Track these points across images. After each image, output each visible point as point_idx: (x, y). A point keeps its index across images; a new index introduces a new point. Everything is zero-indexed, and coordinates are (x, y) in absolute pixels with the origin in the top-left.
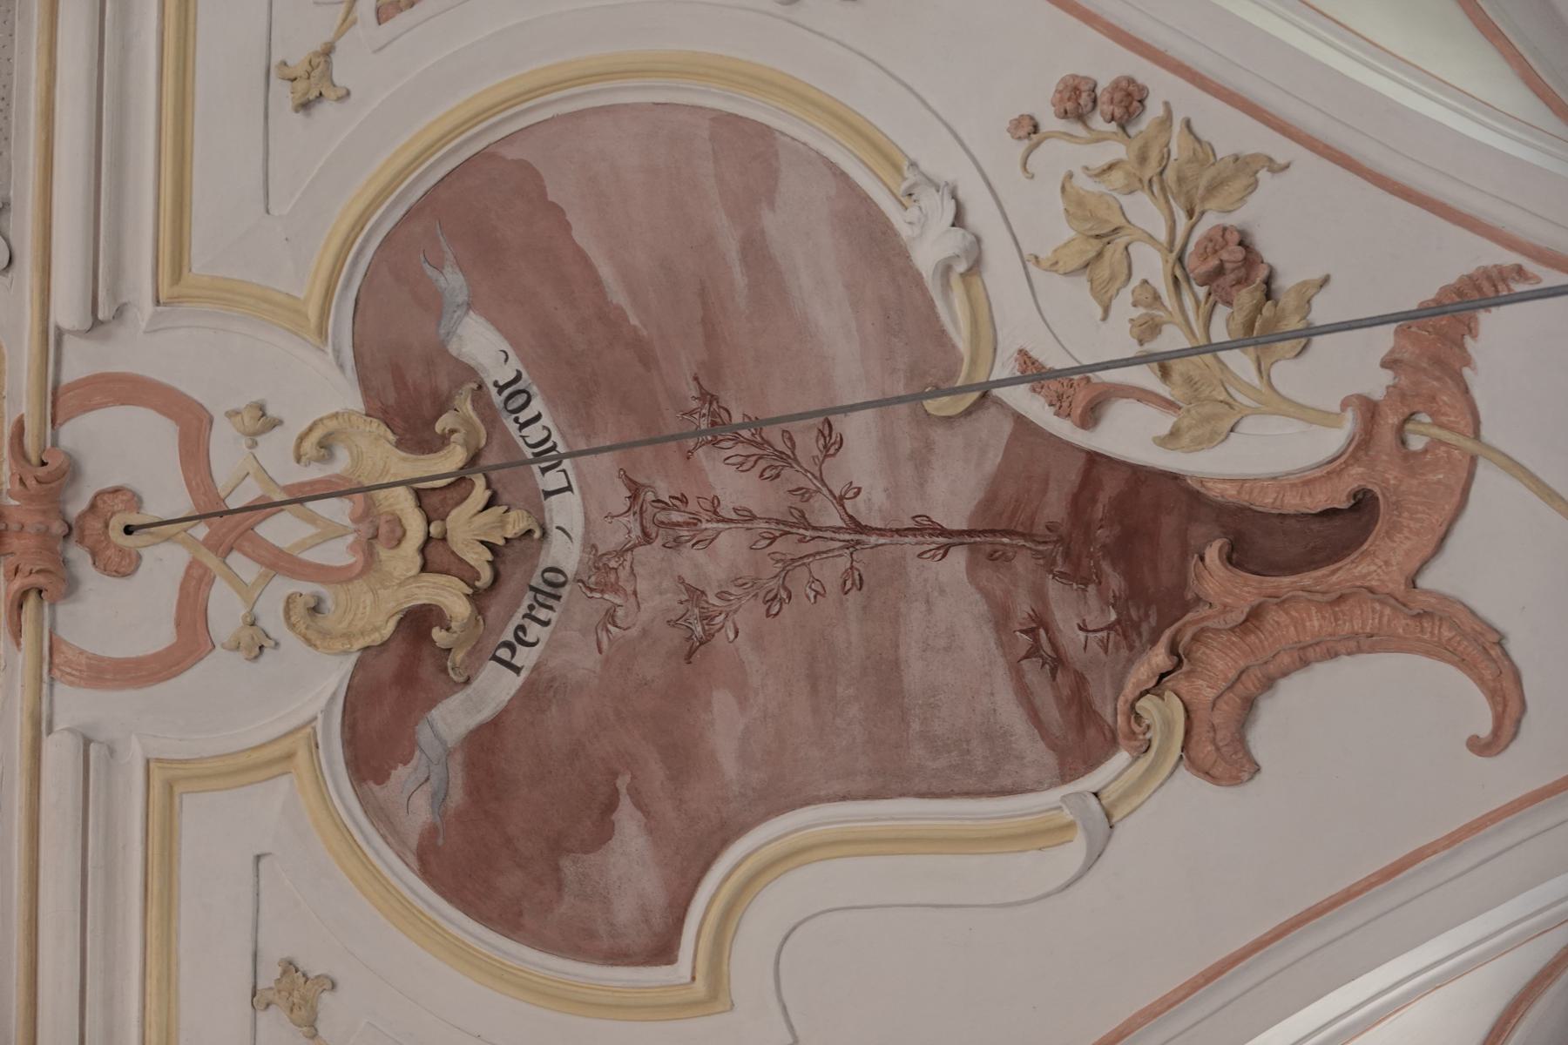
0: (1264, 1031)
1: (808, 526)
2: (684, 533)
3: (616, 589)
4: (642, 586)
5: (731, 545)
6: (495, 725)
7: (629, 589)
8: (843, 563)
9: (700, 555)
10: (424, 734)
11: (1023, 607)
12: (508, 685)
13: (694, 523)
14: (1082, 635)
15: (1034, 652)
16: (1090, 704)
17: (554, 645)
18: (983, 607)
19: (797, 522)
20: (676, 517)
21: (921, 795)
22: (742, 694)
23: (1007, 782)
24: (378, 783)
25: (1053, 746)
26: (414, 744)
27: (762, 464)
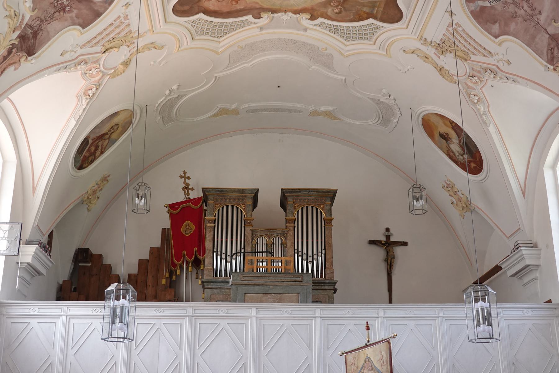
0: (446, 117)
1: (533, 18)
2: (518, 7)
3: (507, 5)
4: (510, 7)
5: (522, 12)
6: (486, 7)
7: (508, 6)
8: (535, 24)
9: (518, 10)
10: (476, 2)
11: (552, 46)
12: (489, 5)
13: (520, 7)
14: (556, 54)
15: (551, 50)
16: (553, 60)
17: (496, 5)
18: (548, 42)
19: (532, 17)
20: (517, 4)
21: (531, 49)
22: (517, 24)
23: (541, 57)
24: (469, 3)
25: (548, 59)
26: (475, 2)
27: (531, 8)
